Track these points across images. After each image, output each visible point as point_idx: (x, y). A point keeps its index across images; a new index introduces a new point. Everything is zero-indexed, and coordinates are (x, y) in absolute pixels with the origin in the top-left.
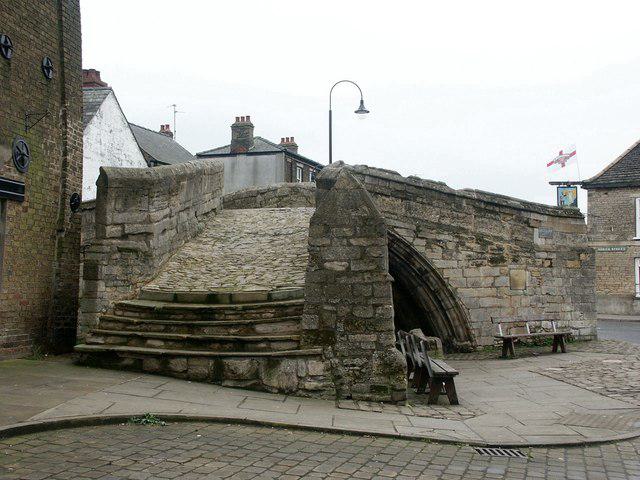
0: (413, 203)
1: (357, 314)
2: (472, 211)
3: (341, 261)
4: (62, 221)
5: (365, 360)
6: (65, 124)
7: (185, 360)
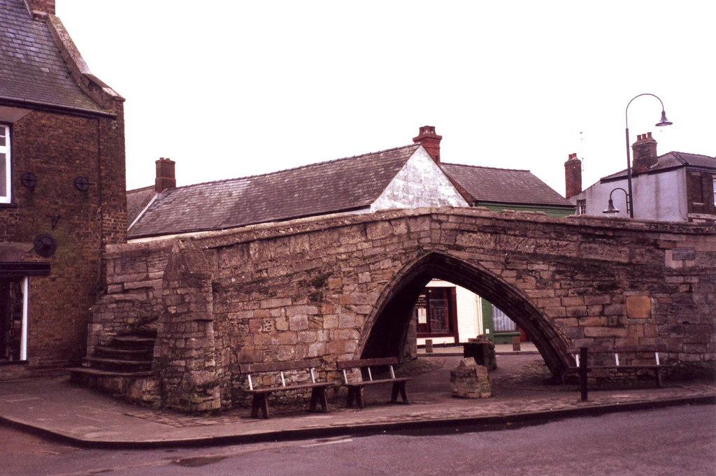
0: (504, 237)
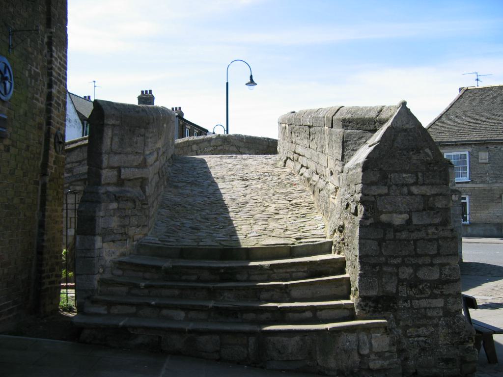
1: (421, 274)
3: (401, 213)
6: (51, 50)
7: (217, 337)
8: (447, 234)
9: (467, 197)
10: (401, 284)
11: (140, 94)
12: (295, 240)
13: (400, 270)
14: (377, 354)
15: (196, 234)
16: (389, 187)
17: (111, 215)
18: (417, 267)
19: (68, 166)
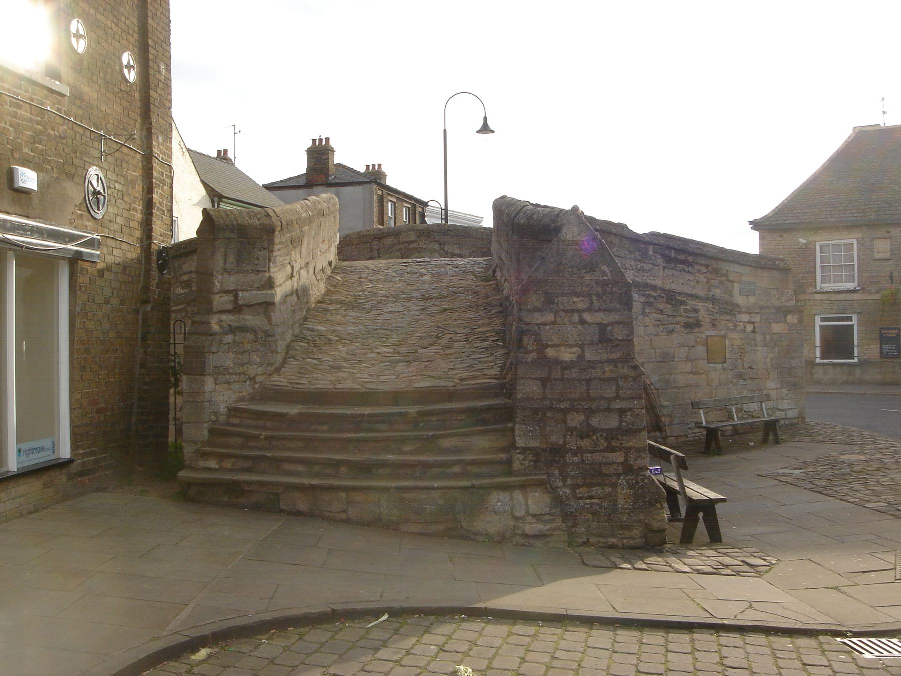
1: (594, 422)
2: (660, 261)
3: (570, 346)
4: (146, 289)
5: (608, 489)
8: (625, 370)
9: (855, 318)
10: (569, 433)
11: (310, 144)
12: (458, 381)
13: (567, 417)
14: (534, 516)
15: (335, 374)
16: (556, 314)
17: (225, 351)
18: (590, 412)
19: (185, 278)
